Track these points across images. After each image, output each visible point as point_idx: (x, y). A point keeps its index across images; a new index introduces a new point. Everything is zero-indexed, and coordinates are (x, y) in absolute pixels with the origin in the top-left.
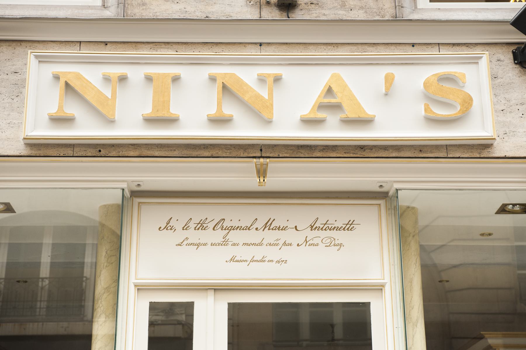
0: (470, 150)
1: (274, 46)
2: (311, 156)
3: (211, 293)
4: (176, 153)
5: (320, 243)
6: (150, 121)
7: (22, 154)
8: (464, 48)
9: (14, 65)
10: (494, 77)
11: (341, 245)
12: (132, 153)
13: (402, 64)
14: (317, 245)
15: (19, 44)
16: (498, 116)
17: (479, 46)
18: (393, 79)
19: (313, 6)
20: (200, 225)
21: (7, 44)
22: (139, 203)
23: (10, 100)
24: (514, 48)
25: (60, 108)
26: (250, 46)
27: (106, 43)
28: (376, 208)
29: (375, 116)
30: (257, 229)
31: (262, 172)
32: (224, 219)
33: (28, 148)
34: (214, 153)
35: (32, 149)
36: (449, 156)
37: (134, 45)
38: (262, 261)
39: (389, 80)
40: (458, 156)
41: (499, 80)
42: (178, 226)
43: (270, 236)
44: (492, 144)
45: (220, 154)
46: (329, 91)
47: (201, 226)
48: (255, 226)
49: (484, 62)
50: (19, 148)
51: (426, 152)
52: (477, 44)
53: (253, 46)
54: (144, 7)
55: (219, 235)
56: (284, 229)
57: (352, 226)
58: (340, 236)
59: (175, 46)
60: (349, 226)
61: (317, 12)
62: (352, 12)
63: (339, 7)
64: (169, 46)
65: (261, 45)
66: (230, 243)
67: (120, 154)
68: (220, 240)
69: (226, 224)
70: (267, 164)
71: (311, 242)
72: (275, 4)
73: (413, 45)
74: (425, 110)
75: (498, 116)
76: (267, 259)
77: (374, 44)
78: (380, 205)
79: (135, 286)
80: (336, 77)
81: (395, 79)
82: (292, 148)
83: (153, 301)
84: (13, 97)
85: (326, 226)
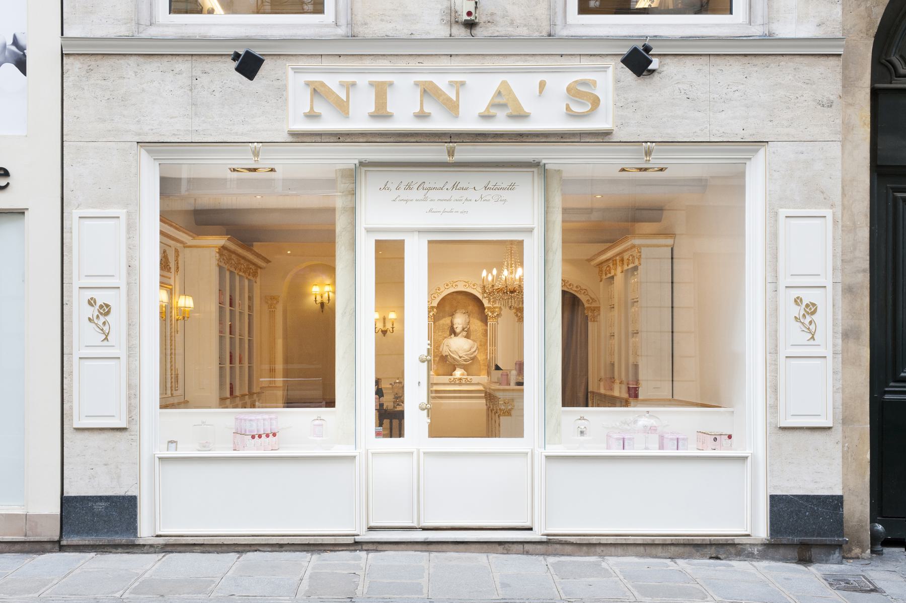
0: (596, 137)
1: (461, 57)
2: (485, 141)
3: (416, 234)
4: (391, 140)
5: (491, 199)
6: (374, 116)
8: (598, 58)
9: (276, 74)
10: (617, 81)
11: (505, 200)
12: (361, 140)
13: (552, 72)
14: (489, 200)
15: (279, 57)
16: (618, 111)
17: (609, 56)
18: (545, 85)
21: (271, 57)
22: (365, 171)
23: (275, 101)
25: (312, 108)
26: (443, 57)
27: (340, 56)
29: (530, 113)
30: (447, 189)
31: (451, 153)
32: (424, 182)
33: (291, 137)
34: (418, 139)
35: (293, 137)
37: (359, 57)
38: (451, 212)
39: (542, 85)
40: (587, 141)
41: (621, 83)
43: (456, 194)
44: (612, 132)
45: (422, 140)
46: (499, 93)
47: (409, 187)
48: (446, 187)
49: (610, 71)
50: (285, 137)
51: (566, 138)
52: (607, 55)
53: (446, 57)
54: (366, 26)
55: (421, 193)
57: (513, 187)
58: (505, 194)
60: (511, 187)
61: (493, 29)
62: (518, 29)
63: (509, 24)
64: (385, 57)
65: (451, 56)
66: (429, 199)
67: (353, 141)
68: (422, 197)
70: (455, 147)
71: (484, 199)
72: (462, 23)
74: (567, 109)
75: (618, 111)
76: (454, 211)
77: (533, 55)
78: (533, 171)
79: (365, 229)
80: (504, 83)
81: (547, 85)
82: (472, 136)
83: (377, 239)
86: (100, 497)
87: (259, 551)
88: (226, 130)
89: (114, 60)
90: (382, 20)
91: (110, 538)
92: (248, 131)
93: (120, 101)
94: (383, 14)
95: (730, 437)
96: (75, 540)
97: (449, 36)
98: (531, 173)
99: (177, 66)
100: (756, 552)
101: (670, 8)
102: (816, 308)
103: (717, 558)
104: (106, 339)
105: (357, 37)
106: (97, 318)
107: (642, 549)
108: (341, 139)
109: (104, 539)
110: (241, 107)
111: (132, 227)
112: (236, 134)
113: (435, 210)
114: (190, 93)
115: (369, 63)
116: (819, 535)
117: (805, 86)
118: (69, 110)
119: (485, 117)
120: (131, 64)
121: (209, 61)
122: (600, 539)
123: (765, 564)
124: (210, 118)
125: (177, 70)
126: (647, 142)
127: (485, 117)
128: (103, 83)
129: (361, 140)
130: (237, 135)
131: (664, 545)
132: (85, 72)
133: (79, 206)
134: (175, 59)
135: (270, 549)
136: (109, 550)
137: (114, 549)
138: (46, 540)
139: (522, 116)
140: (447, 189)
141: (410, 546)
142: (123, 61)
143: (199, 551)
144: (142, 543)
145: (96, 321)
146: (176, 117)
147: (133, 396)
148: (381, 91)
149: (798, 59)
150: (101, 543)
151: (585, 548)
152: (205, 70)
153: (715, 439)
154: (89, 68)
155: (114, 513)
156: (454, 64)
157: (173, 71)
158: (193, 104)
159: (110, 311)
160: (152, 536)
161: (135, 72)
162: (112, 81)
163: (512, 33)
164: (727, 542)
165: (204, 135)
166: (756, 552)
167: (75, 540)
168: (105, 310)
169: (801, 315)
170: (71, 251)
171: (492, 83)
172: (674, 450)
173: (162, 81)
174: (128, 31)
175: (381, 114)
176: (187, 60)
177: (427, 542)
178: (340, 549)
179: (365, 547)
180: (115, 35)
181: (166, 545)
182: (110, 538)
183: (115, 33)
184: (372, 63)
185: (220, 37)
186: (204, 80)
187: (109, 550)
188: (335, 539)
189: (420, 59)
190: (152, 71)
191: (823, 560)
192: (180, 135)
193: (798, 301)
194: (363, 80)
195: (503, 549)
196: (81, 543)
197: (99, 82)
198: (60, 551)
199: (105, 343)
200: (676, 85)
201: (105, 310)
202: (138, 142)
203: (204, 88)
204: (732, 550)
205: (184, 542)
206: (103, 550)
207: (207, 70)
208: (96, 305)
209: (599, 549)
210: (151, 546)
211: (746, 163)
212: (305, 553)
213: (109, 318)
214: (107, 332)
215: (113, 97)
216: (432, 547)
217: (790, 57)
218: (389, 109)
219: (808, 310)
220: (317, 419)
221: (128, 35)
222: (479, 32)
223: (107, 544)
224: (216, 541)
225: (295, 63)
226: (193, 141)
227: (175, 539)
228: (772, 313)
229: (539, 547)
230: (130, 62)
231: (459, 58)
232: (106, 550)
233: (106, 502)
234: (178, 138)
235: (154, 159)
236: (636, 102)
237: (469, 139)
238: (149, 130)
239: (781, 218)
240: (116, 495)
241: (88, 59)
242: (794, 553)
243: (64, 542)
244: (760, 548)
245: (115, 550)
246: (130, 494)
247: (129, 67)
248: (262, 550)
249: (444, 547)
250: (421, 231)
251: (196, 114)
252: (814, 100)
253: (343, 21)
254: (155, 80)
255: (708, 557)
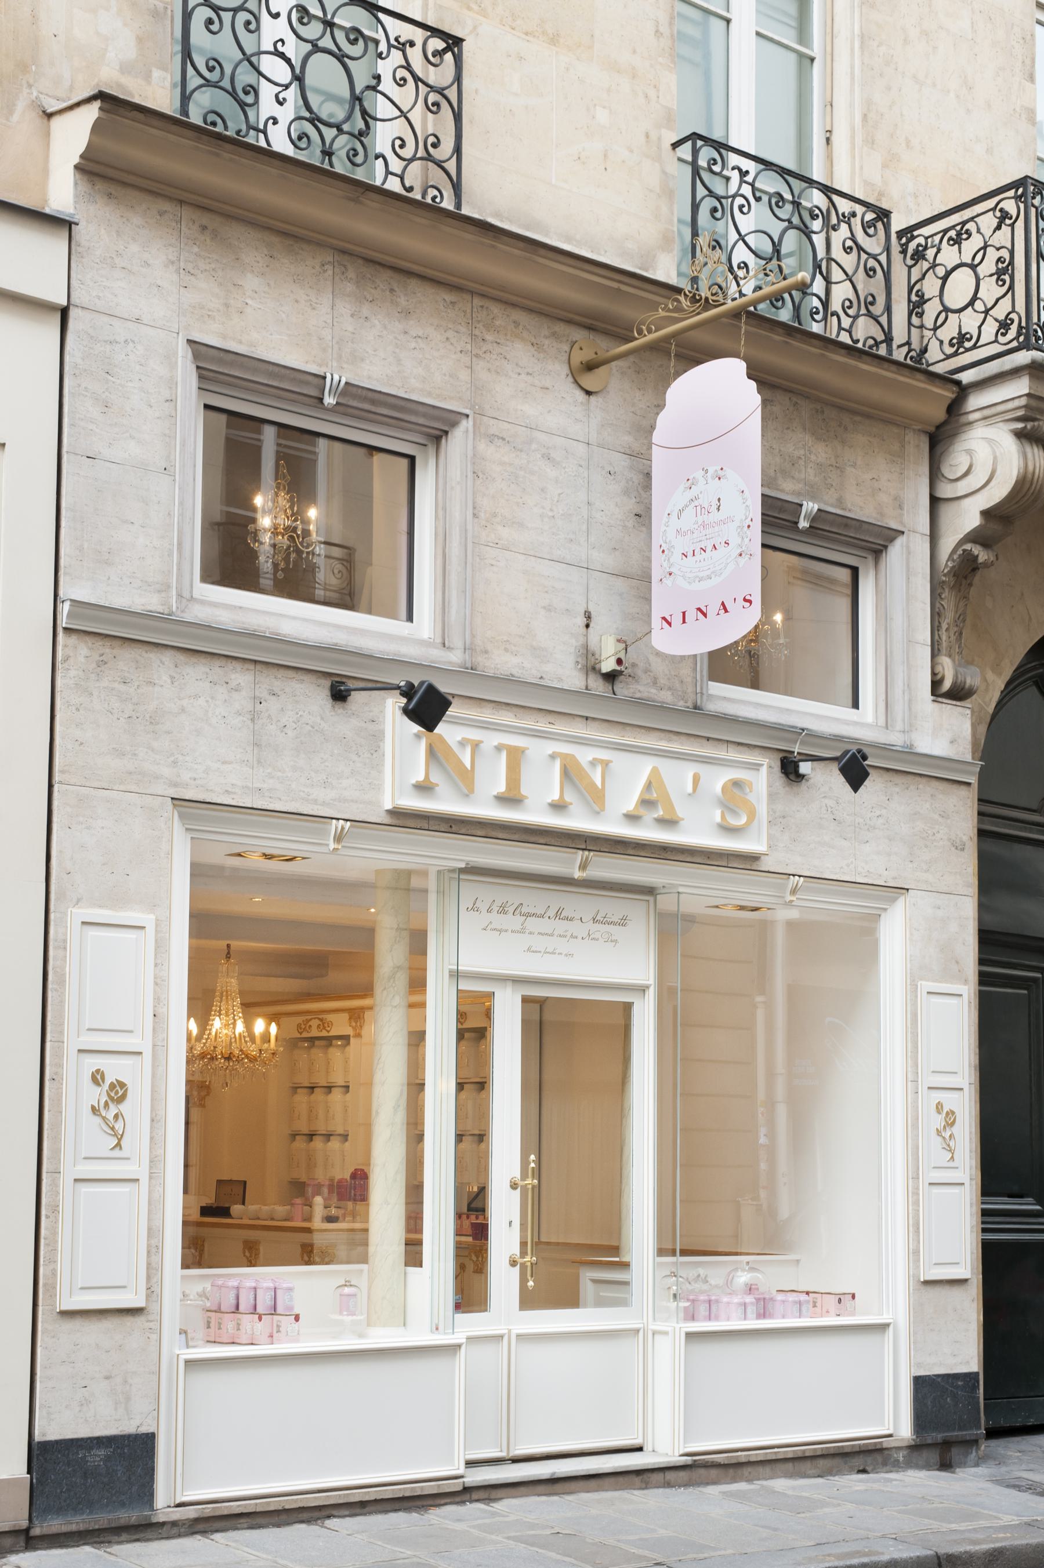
3: (510, 984)
4: (516, 837)
7: (384, 822)
9: (370, 711)
11: (616, 941)
12: (479, 833)
19: (631, 678)
20: (502, 908)
22: (450, 878)
23: (369, 755)
24: (782, 755)
28: (644, 904)
29: (527, 798)
35: (392, 818)
36: (729, 865)
42: (484, 908)
43: (561, 926)
47: (503, 910)
48: (547, 915)
54: (487, 656)
56: (571, 920)
59: (515, 709)
60: (623, 922)
64: (508, 708)
65: (587, 719)
66: (528, 931)
68: (518, 927)
69: (524, 910)
73: (708, 739)
76: (557, 951)
77: (678, 732)
78: (648, 901)
84: (372, 752)
85: (605, 919)
86: (98, 1439)
87: (335, 1516)
88: (302, 794)
89: (140, 650)
90: (506, 650)
91: (111, 1516)
92: (332, 800)
93: (148, 723)
94: (508, 641)
95: (853, 1297)
96: (55, 1525)
97: (584, 688)
98: (644, 903)
99: (233, 676)
100: (901, 1459)
101: (272, 584)
102: (126, 1090)
103: (864, 1471)
104: (118, 1145)
105: (475, 670)
106: (105, 1107)
107: (789, 1466)
108: (454, 829)
109: (102, 1519)
110: (322, 758)
111: (161, 946)
112: (315, 802)
113: (535, 949)
114: (251, 726)
115: (490, 714)
116: (960, 1429)
117: (940, 820)
118: (67, 728)
119: (632, 818)
120: (166, 663)
121: (280, 676)
122: (749, 1455)
123: (911, 1473)
124: (280, 771)
125: (233, 684)
126: (338, 819)
127: (632, 818)
128: (123, 688)
129: (479, 833)
130: (317, 805)
131: (814, 1457)
132: (94, 665)
133: (78, 901)
134: (232, 665)
135: (347, 1513)
136: (106, 1539)
137: (115, 1535)
138: (7, 1530)
139: (669, 822)
140: (549, 917)
141: (531, 1488)
142: (153, 657)
143: (245, 1526)
144: (161, 1520)
145: (104, 1113)
146: (230, 763)
147: (154, 1250)
148: (515, 758)
149: (935, 784)
150: (97, 1527)
151: (731, 1471)
152: (273, 690)
153: (840, 1301)
154: (101, 658)
155: (119, 1468)
156: (590, 731)
157: (227, 683)
158: (255, 744)
159: (126, 1095)
160: (169, 1507)
161: (172, 678)
162: (136, 687)
163: (656, 697)
164: (876, 1446)
165: (270, 797)
166: (901, 1459)
167: (55, 1525)
168: (118, 1092)
169: (942, 1127)
170: (62, 982)
171: (642, 768)
172: (796, 1317)
173: (212, 698)
174: (162, 605)
175: (511, 799)
176: (248, 669)
177: (554, 1479)
178: (443, 1502)
179: (475, 1496)
180: (143, 608)
181: (197, 1520)
182: (111, 1516)
183: (143, 605)
184: (494, 714)
185: (299, 640)
186: (272, 705)
187: (106, 1539)
188: (439, 1486)
189: (551, 718)
190: (197, 680)
191: (962, 1463)
192: (235, 793)
193: (97, 1078)
194: (491, 740)
195: (642, 1481)
196: (65, 1529)
197: (116, 685)
198: (26, 1548)
199: (117, 1153)
200: (823, 800)
201: (118, 1092)
202: (172, 798)
203: (272, 719)
204: (879, 1458)
205: (226, 1513)
206: (97, 1539)
207: (276, 690)
208: (103, 1082)
209: (746, 1471)
210: (174, 1524)
211: (880, 916)
212: (198, 1537)
213: (124, 1107)
214: (121, 1133)
215: (138, 715)
216: (558, 1487)
217: (928, 779)
218: (524, 791)
219: (113, 1094)
220: (346, 1285)
221: (162, 611)
222: (623, 689)
223: (107, 1526)
224: (274, 1504)
225: (615, 735)
226: (255, 807)
227: (213, 1508)
228: (913, 1124)
229: (682, 1474)
230: (164, 659)
231: (596, 724)
232: (102, 1539)
233: (107, 1447)
234: (233, 799)
235: (187, 829)
236: (784, 817)
237: (606, 848)
238: (190, 778)
239: (922, 994)
240: (122, 1433)
241: (99, 643)
242: (934, 1456)
243: (36, 1531)
244: (905, 1453)
245: (116, 1537)
246: (144, 1429)
247: (162, 664)
248: (336, 1514)
249: (573, 1485)
250: (517, 981)
251: (259, 762)
252: (949, 839)
253: (457, 641)
254: (200, 695)
255: (856, 1471)
